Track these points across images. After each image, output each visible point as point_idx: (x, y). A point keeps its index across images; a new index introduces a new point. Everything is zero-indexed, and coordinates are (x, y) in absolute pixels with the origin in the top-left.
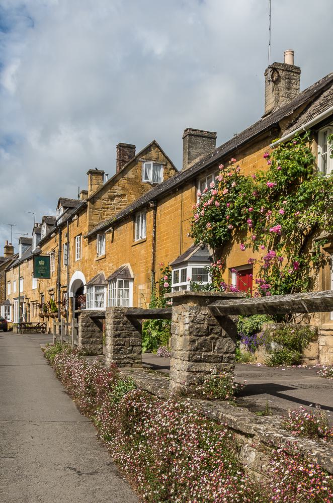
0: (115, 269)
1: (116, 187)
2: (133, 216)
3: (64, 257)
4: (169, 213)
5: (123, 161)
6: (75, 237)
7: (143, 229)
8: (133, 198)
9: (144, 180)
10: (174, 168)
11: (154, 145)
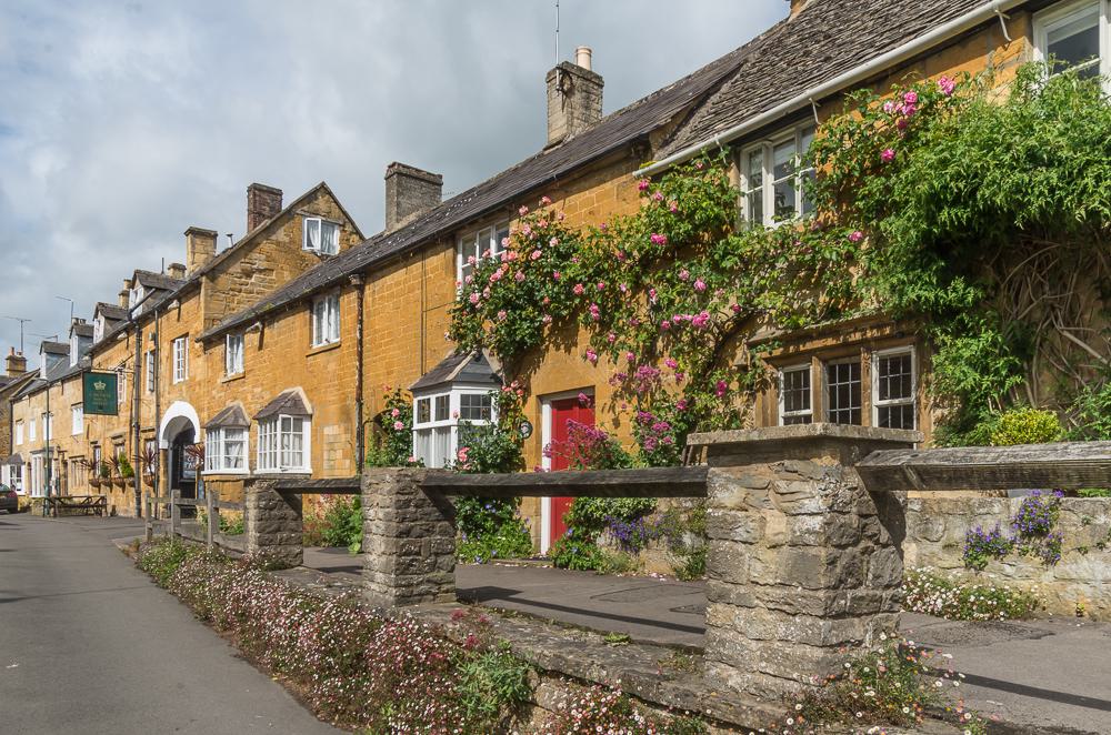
0: (268, 397)
1: (255, 255)
2: (308, 301)
3: (147, 376)
4: (392, 296)
5: (260, 214)
6: (173, 341)
7: (330, 326)
8: (288, 277)
9: (306, 248)
10: (358, 232)
11: (322, 190)
